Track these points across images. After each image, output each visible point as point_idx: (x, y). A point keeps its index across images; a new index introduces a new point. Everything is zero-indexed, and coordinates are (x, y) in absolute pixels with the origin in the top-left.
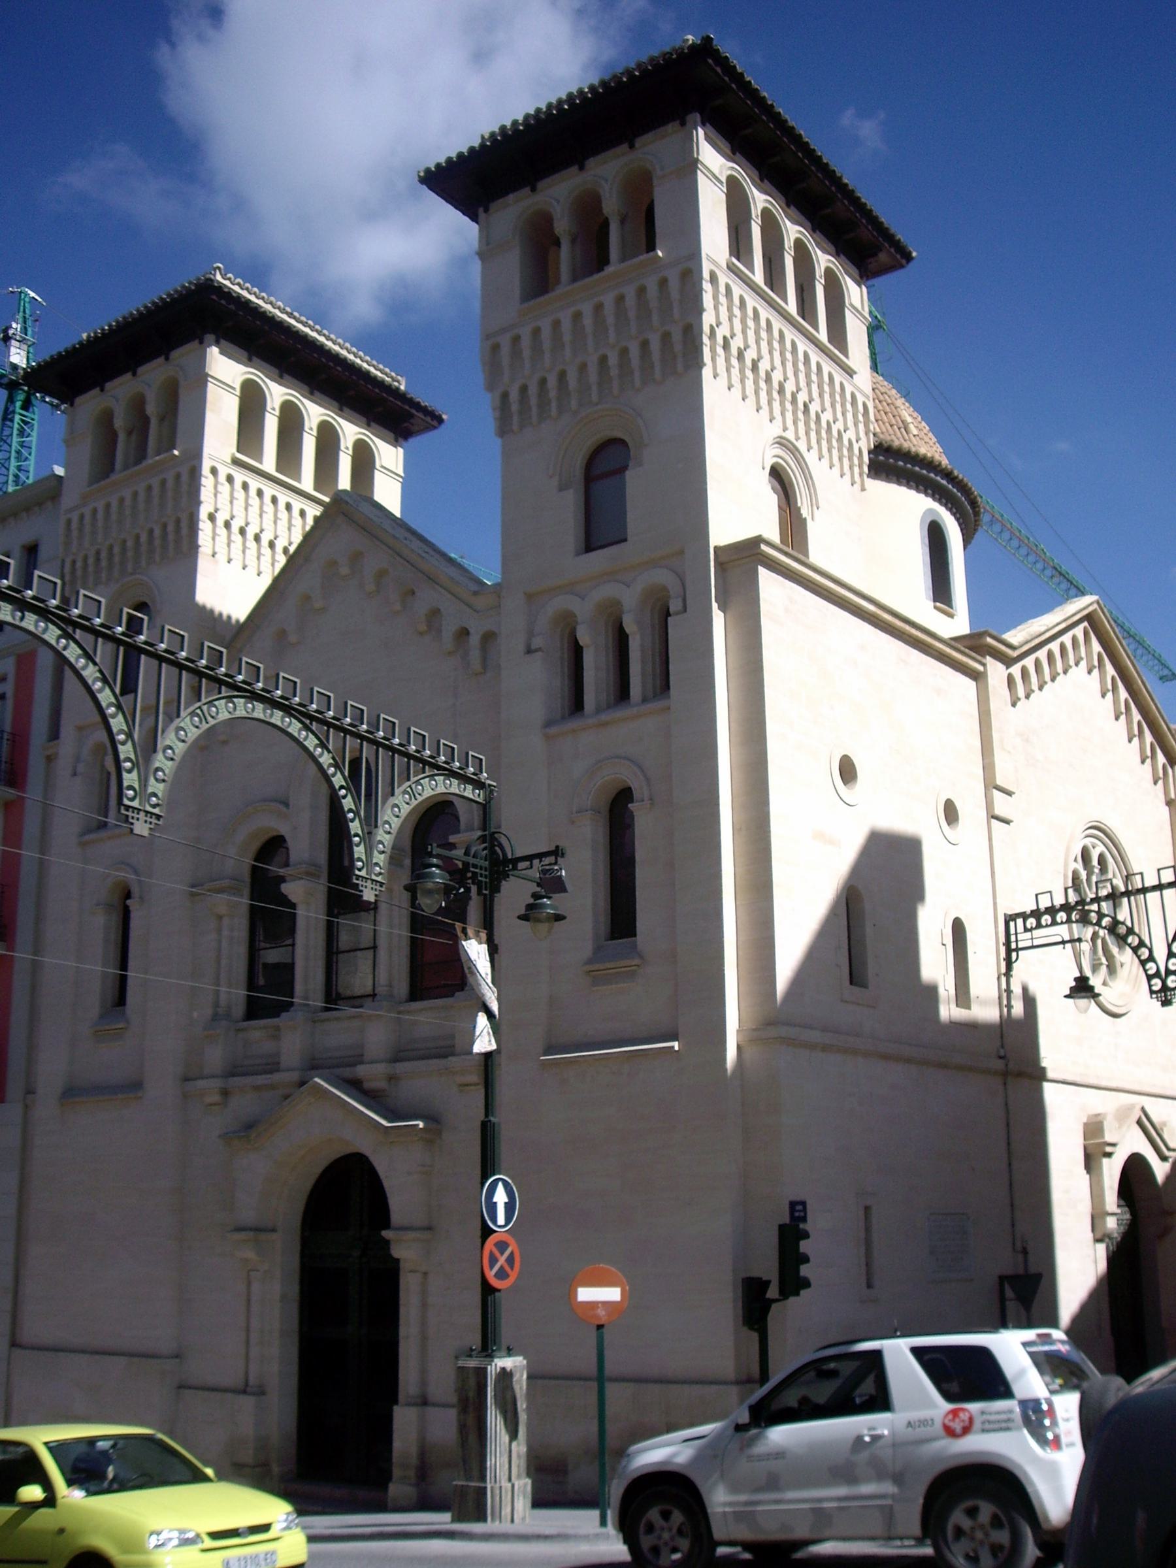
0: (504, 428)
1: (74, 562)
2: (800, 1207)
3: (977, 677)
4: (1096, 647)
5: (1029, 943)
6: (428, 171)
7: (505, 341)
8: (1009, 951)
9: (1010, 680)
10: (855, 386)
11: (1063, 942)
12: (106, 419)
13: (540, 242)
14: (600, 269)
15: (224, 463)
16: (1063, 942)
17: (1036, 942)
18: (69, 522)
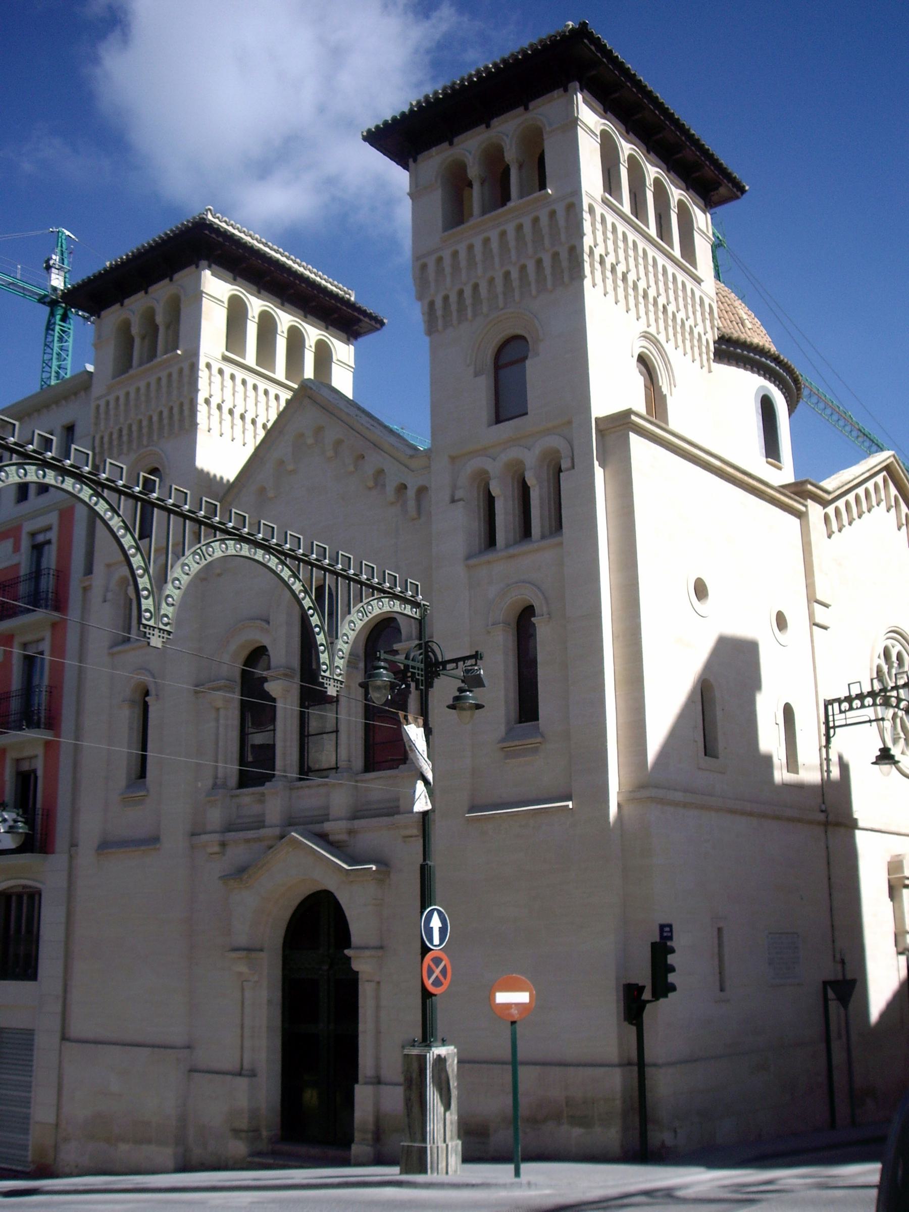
0: (431, 328)
1: (102, 438)
2: (667, 929)
3: (800, 515)
4: (893, 491)
5: (843, 722)
6: (369, 131)
7: (431, 262)
8: (828, 728)
9: (826, 518)
10: (702, 291)
11: (870, 721)
12: (125, 327)
13: (457, 183)
14: (503, 204)
15: (216, 360)
16: (870, 721)
17: (849, 722)
18: (98, 407)
